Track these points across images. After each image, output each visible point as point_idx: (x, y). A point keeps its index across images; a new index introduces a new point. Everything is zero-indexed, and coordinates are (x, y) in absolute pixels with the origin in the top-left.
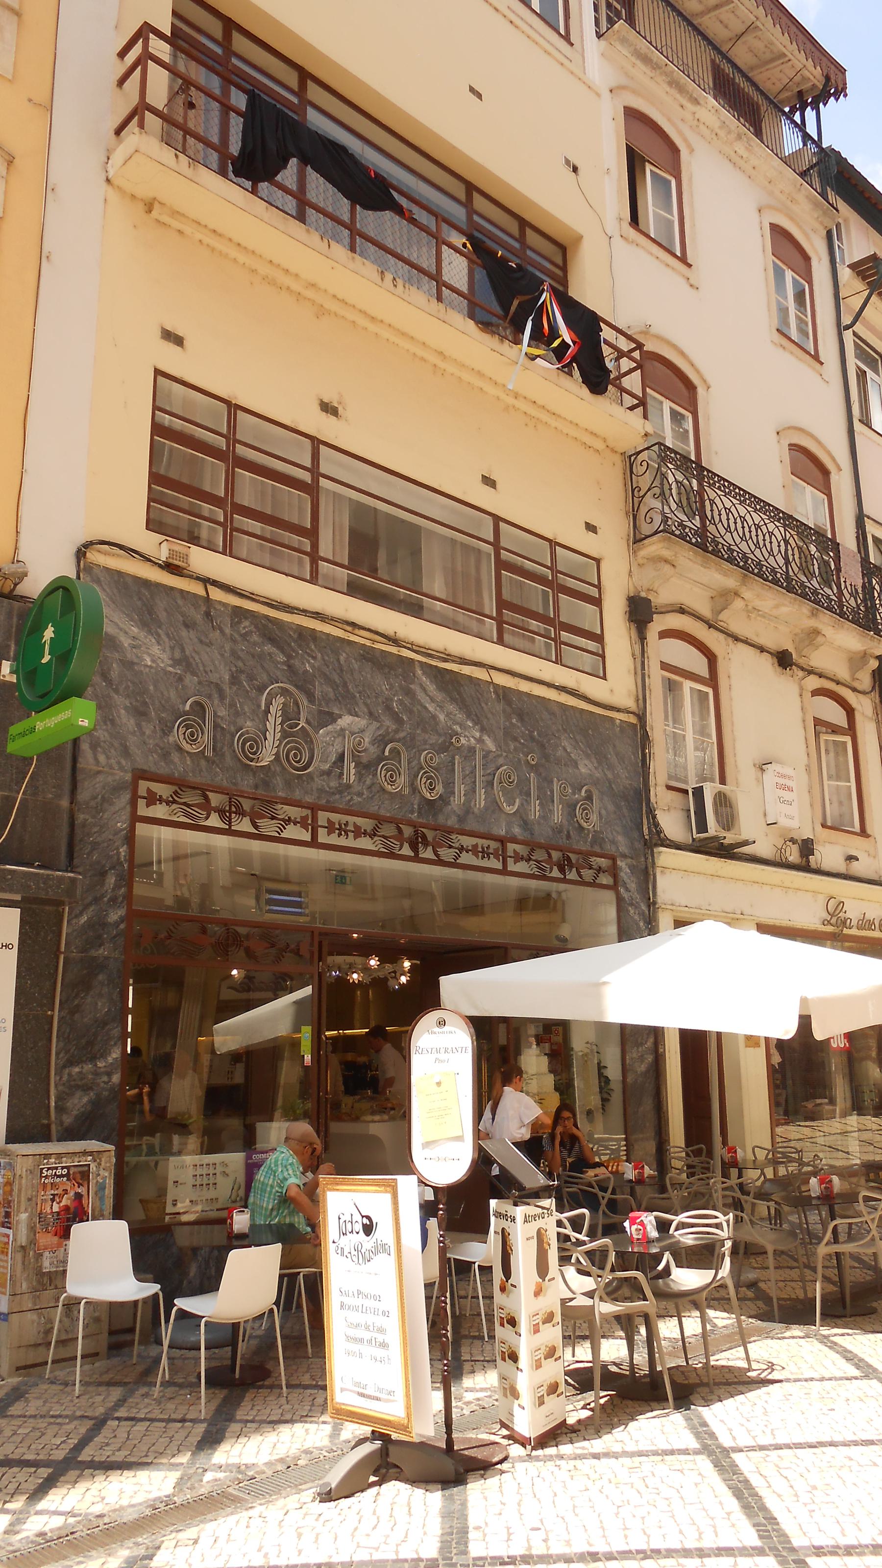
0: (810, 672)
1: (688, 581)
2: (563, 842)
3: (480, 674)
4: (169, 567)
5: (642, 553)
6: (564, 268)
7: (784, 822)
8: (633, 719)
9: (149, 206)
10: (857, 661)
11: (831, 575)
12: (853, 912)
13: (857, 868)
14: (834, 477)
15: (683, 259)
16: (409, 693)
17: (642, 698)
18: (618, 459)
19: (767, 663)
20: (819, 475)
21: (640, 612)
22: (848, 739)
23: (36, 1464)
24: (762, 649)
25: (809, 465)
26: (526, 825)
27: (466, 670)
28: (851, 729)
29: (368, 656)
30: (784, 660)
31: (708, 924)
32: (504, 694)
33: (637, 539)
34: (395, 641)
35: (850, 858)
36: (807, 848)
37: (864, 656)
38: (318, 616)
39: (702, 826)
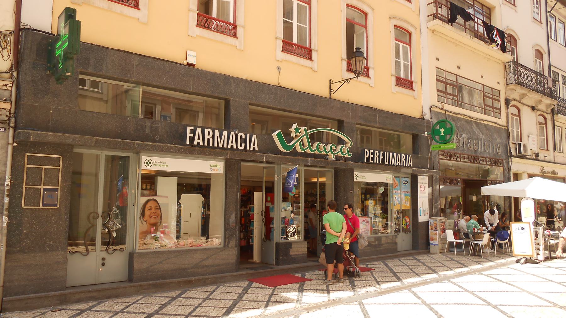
0: (538, 110)
1: (517, 92)
2: (495, 157)
3: (482, 122)
4: (441, 109)
5: (509, 88)
6: (490, 15)
7: (533, 149)
8: (506, 128)
9: (433, 31)
10: (548, 106)
11: (543, 84)
12: (546, 170)
13: (546, 159)
14: (544, 56)
15: (514, 5)
16: (472, 128)
17: (508, 123)
18: (503, 64)
19: (530, 109)
20: (540, 55)
21: (507, 102)
22: (545, 126)
23: (110, 312)
24: (529, 106)
25: (539, 54)
26: (489, 154)
27: (480, 121)
28: (546, 123)
29: (467, 121)
30: (533, 108)
31: (537, 178)
32: (486, 125)
33: (507, 84)
34: (470, 117)
35: (545, 157)
36: (537, 155)
37: (550, 105)
38: (460, 114)
39: (520, 152)
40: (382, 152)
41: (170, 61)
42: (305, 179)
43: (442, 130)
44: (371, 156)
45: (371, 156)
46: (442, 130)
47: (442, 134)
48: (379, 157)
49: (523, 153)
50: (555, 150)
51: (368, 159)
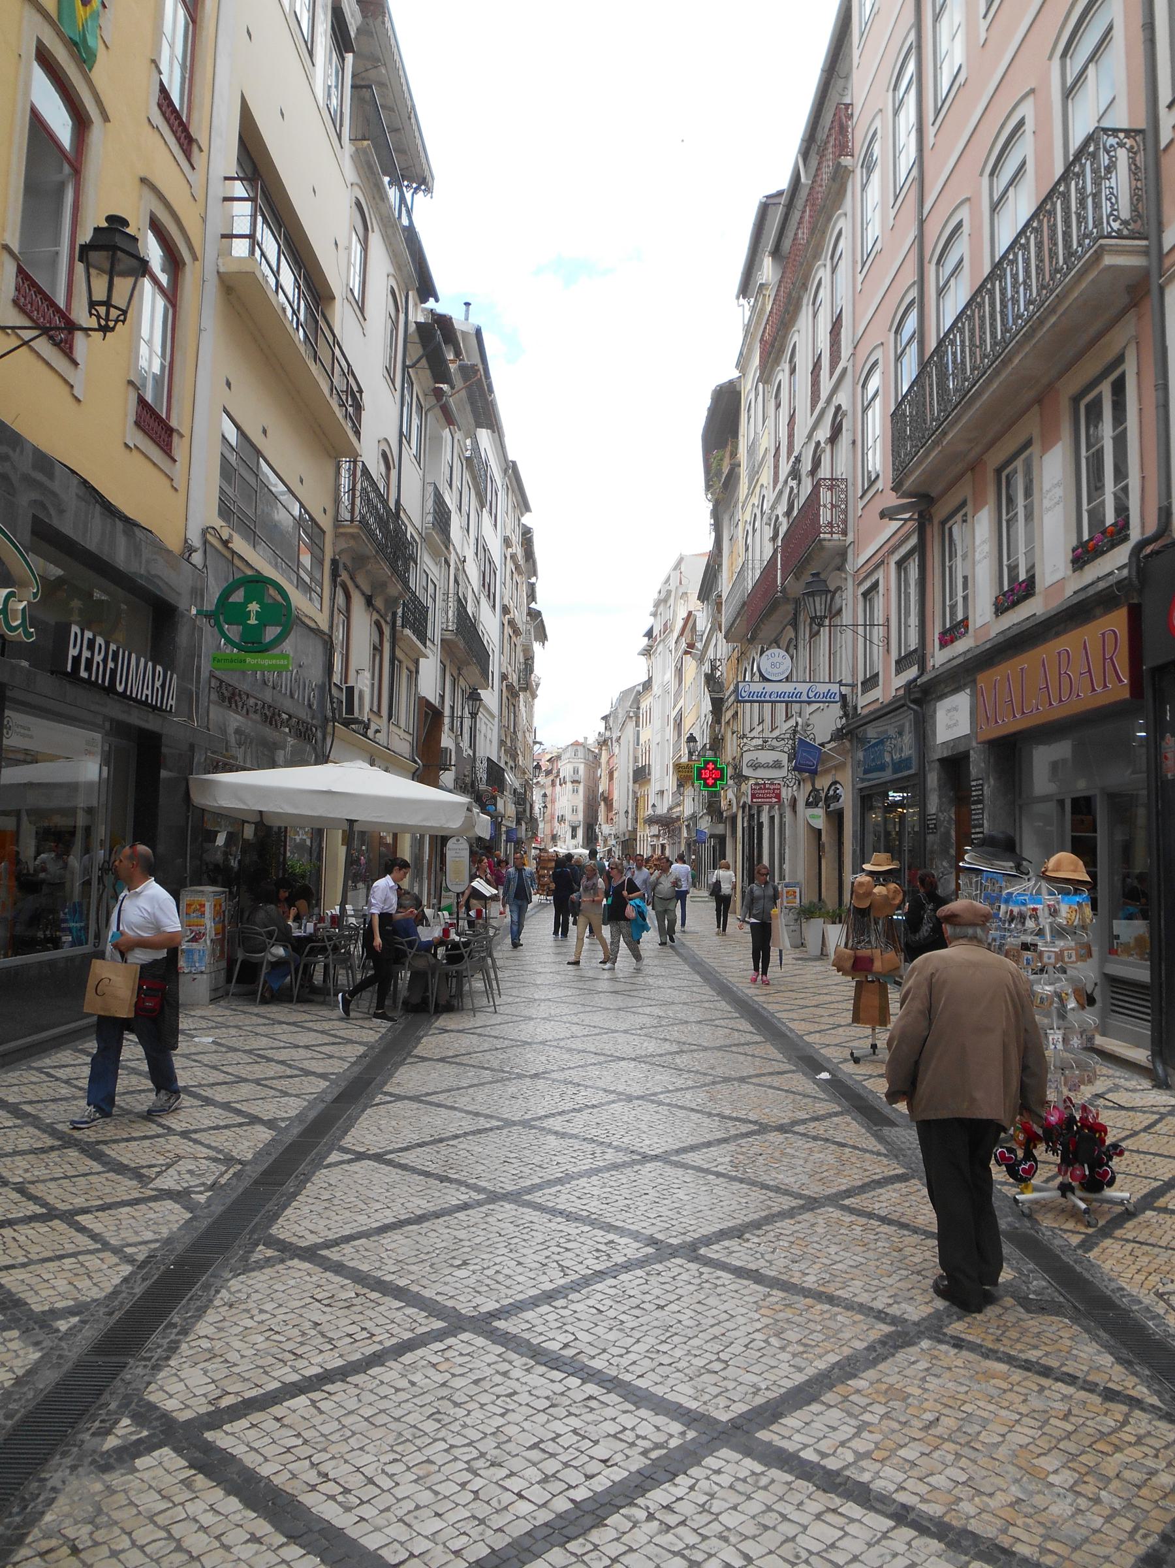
40: (113, 647)
41: (40, 785)
42: (354, 76)
43: (254, 607)
44: (86, 654)
45: (86, 654)
46: (254, 607)
47: (253, 621)
48: (105, 660)
49: (356, 715)
50: (390, 717)
51: (77, 659)
